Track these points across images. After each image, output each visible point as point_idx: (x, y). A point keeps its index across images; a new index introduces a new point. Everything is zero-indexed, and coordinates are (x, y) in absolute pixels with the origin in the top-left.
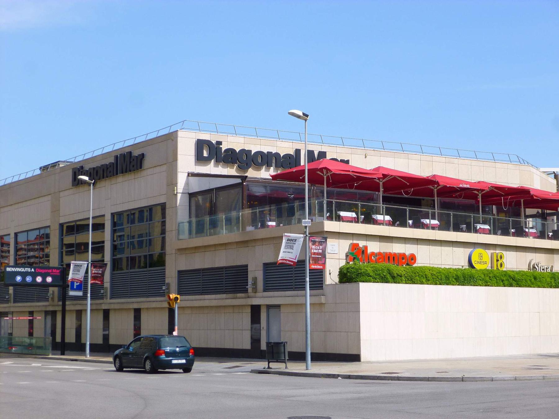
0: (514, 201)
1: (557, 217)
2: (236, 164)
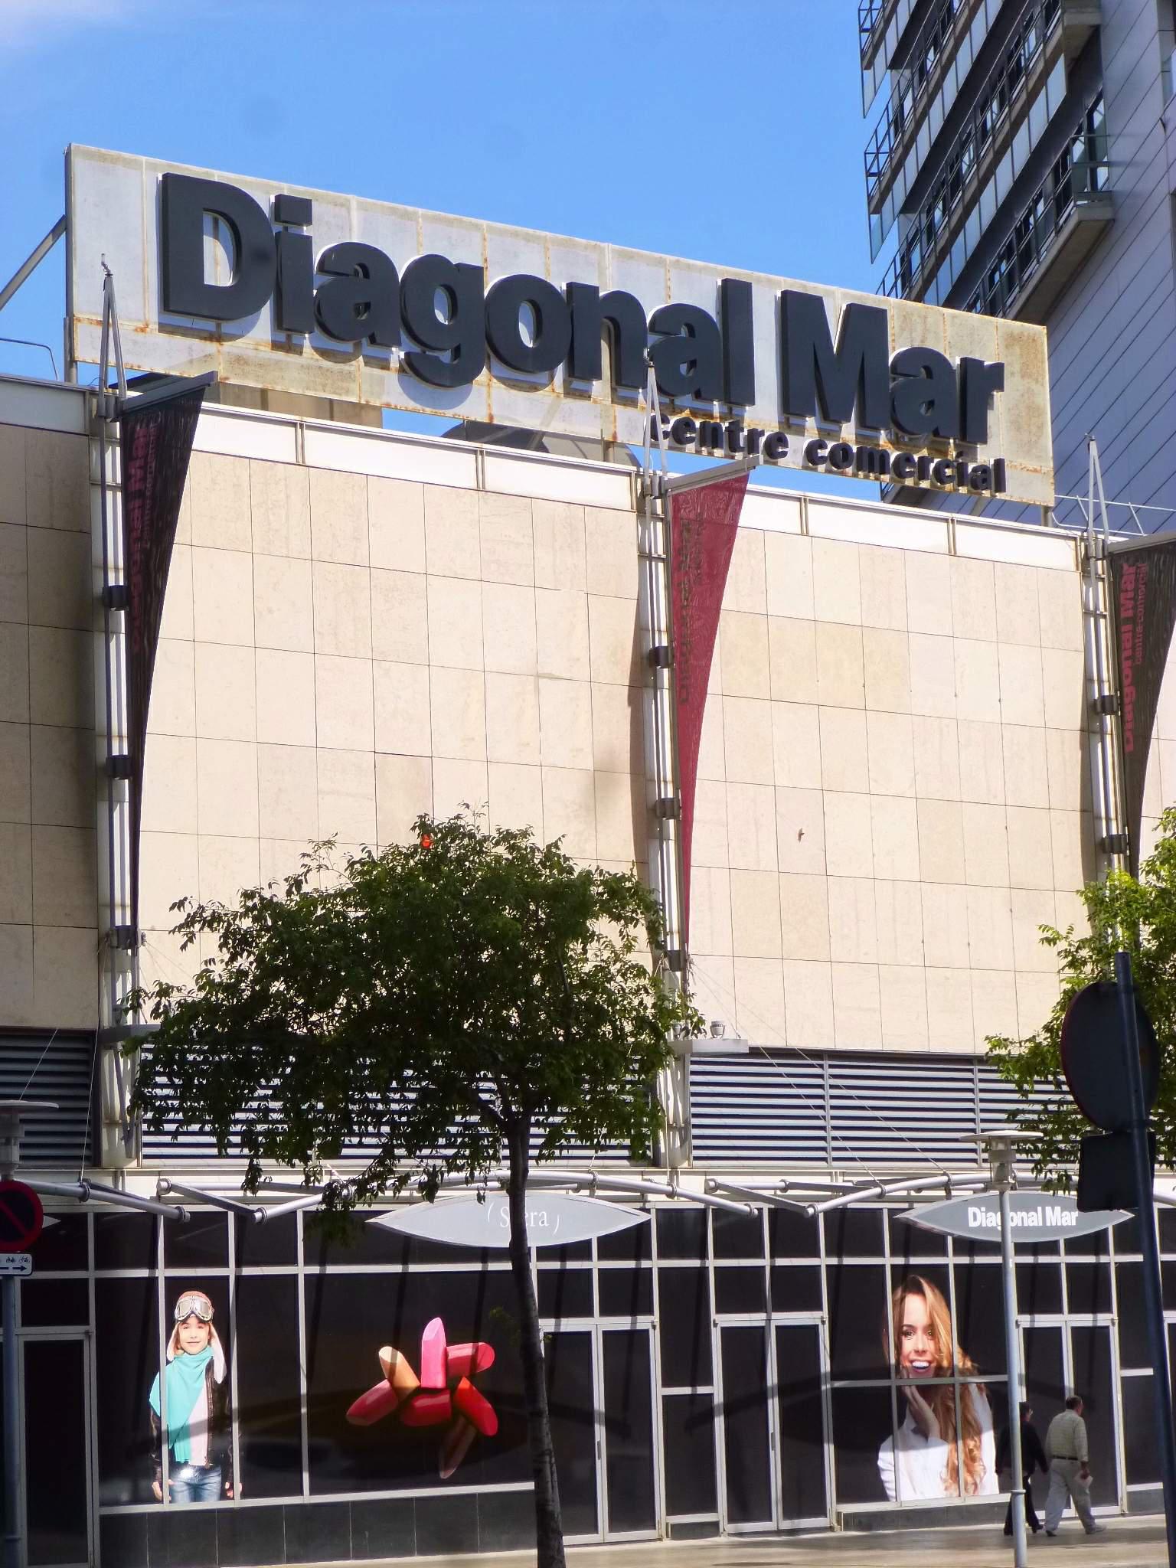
0: (1138, 510)
1: (129, 782)
2: (398, 344)
